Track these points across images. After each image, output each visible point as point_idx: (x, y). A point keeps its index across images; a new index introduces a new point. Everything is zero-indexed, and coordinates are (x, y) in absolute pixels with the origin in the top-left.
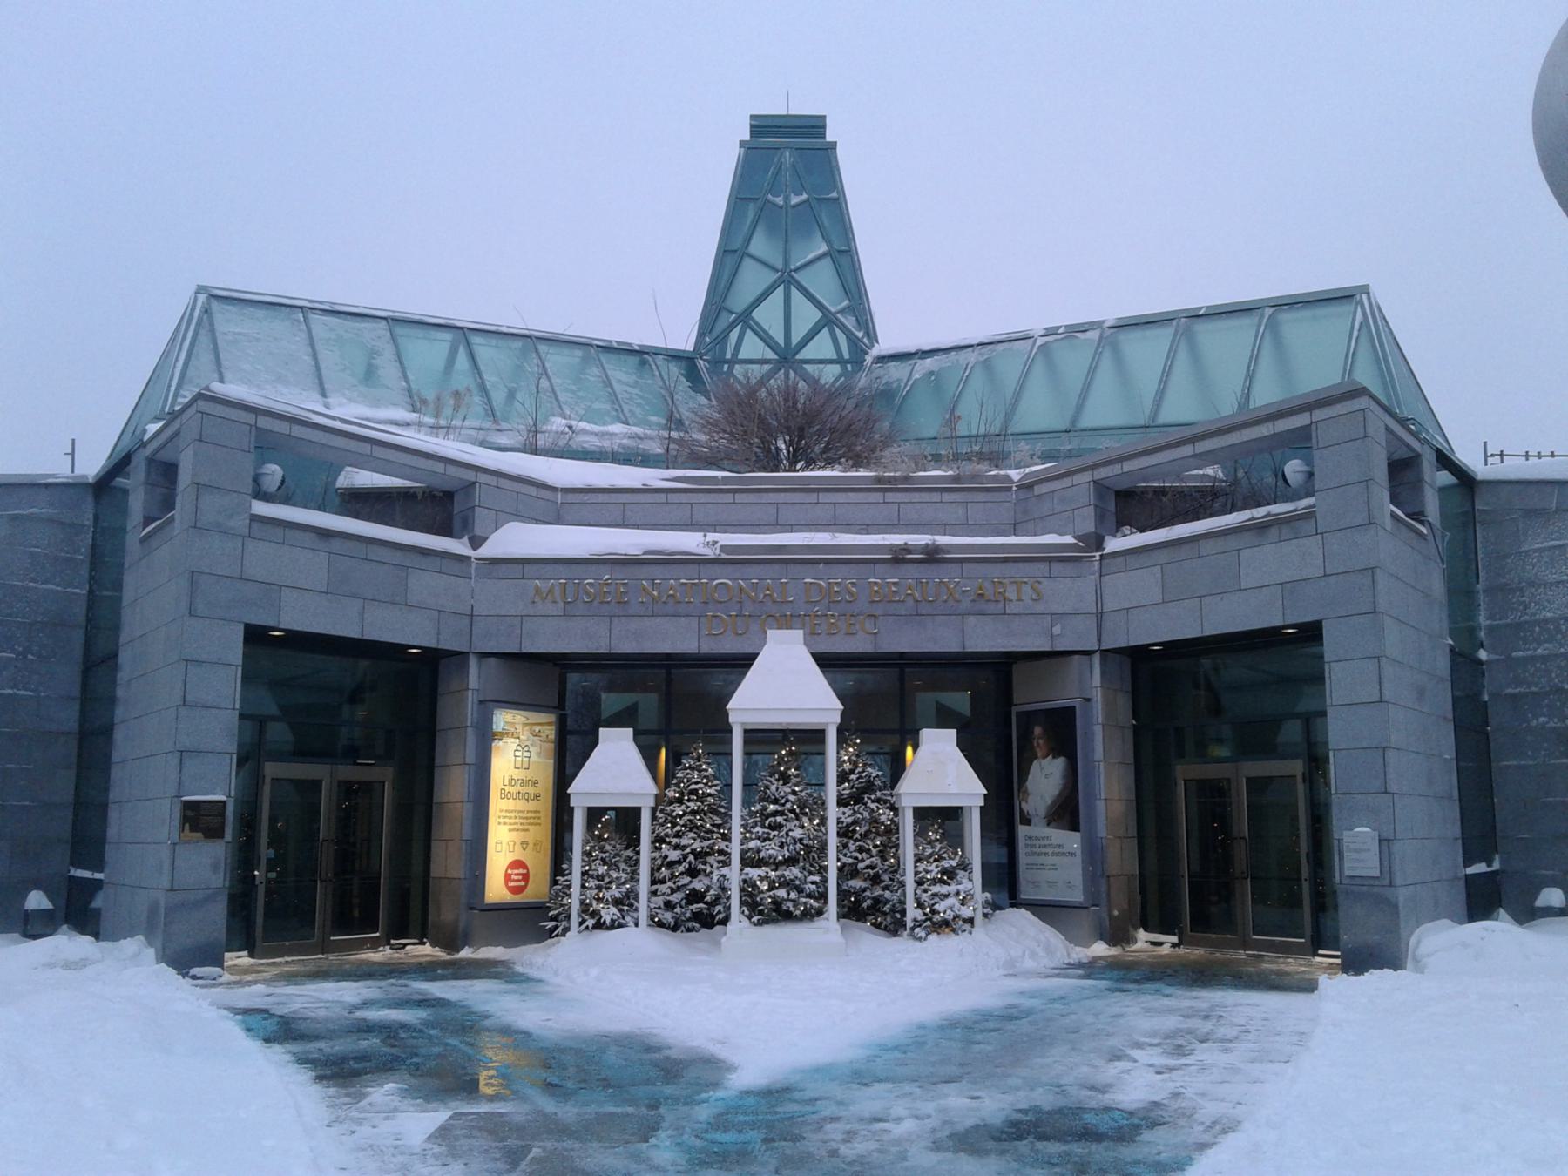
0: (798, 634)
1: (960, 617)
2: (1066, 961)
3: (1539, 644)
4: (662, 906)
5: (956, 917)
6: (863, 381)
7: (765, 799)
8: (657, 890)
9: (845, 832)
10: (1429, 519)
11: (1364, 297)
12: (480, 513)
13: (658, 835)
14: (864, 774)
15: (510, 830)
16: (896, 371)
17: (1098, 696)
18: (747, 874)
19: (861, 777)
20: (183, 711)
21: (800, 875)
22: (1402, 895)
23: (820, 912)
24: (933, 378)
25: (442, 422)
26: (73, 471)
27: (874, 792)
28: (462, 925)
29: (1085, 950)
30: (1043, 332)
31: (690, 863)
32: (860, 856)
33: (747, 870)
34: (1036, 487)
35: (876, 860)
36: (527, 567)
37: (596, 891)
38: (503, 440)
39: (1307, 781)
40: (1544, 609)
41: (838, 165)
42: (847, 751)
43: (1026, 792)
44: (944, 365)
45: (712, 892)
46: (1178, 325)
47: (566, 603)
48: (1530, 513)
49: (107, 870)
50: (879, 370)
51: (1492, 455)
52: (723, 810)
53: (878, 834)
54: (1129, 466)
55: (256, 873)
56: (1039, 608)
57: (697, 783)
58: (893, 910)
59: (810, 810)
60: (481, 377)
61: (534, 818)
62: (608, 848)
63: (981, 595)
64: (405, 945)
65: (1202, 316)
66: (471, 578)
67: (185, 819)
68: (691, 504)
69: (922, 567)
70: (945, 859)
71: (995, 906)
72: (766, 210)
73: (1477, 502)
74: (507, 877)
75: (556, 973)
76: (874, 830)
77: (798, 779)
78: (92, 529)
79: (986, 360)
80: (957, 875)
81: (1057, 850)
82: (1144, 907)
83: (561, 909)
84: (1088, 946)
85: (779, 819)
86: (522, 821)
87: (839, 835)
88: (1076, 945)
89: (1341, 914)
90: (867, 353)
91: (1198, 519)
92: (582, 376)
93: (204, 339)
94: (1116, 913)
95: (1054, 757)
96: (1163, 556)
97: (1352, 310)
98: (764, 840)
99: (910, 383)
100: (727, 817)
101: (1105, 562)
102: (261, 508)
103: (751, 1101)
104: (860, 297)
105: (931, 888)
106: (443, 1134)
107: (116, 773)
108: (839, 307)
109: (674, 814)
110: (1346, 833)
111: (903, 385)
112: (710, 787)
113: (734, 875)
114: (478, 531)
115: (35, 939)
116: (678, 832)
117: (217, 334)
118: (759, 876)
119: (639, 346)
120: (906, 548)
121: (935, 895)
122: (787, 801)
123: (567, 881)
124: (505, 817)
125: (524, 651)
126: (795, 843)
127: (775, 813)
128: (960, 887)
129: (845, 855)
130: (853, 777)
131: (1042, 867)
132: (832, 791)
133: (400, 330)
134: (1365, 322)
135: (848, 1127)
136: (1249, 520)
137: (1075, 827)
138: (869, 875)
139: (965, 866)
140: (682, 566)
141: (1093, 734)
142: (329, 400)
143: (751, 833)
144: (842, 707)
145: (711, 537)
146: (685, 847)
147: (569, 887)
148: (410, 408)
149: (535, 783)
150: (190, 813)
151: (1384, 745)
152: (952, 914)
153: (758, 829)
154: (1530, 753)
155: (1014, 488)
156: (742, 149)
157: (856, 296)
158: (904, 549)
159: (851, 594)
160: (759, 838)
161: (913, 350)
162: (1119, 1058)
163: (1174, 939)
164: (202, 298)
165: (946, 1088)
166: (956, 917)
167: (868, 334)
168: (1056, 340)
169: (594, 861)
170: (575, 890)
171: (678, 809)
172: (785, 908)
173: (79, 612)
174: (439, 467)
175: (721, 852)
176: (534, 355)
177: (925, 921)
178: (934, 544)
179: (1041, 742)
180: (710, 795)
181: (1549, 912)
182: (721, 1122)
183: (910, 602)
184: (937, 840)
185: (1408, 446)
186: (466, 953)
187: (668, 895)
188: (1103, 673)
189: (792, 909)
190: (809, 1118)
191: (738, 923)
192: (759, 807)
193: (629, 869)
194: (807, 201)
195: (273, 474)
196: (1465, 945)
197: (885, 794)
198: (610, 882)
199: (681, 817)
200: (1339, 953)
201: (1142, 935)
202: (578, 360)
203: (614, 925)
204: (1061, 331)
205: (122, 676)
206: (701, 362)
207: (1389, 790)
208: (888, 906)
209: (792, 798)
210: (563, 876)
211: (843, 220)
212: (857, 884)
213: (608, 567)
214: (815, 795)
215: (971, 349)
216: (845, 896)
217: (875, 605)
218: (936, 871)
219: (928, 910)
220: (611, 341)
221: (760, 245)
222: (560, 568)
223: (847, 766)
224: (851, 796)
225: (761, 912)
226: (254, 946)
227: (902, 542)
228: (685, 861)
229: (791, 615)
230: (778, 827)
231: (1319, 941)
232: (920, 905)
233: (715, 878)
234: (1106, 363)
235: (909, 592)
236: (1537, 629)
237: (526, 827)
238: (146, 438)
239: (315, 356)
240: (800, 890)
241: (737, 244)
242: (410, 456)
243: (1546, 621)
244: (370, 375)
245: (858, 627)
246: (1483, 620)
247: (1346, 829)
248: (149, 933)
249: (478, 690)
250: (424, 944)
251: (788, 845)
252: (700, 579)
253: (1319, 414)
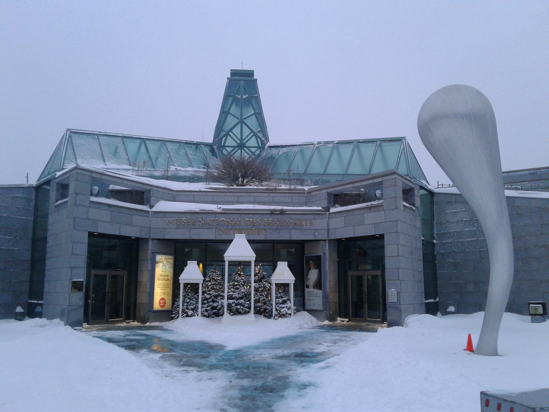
1: (289, 230)
2: (316, 325)
6: (264, 154)
7: (234, 281)
9: (256, 290)
10: (416, 205)
11: (404, 140)
12: (152, 198)
13: (203, 291)
14: (262, 274)
15: (161, 289)
16: (274, 151)
17: (327, 252)
18: (229, 302)
21: (243, 302)
22: (403, 307)
23: (249, 312)
25: (140, 169)
26: (27, 183)
27: (265, 279)
29: (323, 323)
31: (213, 299)
32: (260, 297)
33: (229, 300)
34: (312, 193)
35: (265, 298)
36: (166, 214)
38: (157, 174)
42: (257, 267)
45: (219, 307)
48: (448, 202)
51: (440, 185)
52: (222, 284)
53: (266, 290)
54: (337, 189)
55: (89, 301)
56: (312, 228)
57: (215, 276)
58: (269, 312)
59: (247, 284)
60: (149, 154)
61: (167, 286)
62: (190, 294)
63: (296, 224)
64: (130, 322)
67: (73, 286)
69: (280, 215)
70: (283, 297)
71: (298, 311)
73: (434, 199)
74: (160, 303)
76: (264, 290)
79: (301, 150)
80: (287, 302)
81: (316, 295)
83: (176, 311)
84: (323, 321)
85: (238, 286)
86: (164, 287)
87: (254, 291)
88: (320, 321)
89: (387, 312)
93: (70, 146)
96: (345, 214)
98: (234, 292)
99: (278, 155)
100: (223, 286)
102: (93, 199)
103: (231, 352)
104: (264, 127)
106: (161, 357)
107: (47, 273)
108: (257, 131)
109: (208, 285)
111: (276, 156)
112: (218, 277)
113: (225, 302)
114: (152, 204)
116: (209, 290)
117: (73, 144)
118: (232, 302)
119: (196, 142)
120: (275, 210)
121: (281, 307)
122: (240, 281)
125: (165, 238)
126: (242, 293)
127: (237, 285)
129: (256, 296)
130: (259, 275)
131: (311, 300)
132: (253, 279)
133: (125, 140)
134: (403, 148)
135: (254, 356)
137: (320, 289)
138: (263, 302)
143: (230, 290)
144: (256, 256)
145: (220, 206)
146: (211, 294)
148: (129, 164)
149: (168, 276)
151: (399, 267)
152: (285, 312)
153: (232, 289)
155: (306, 193)
157: (262, 127)
159: (259, 223)
160: (232, 292)
162: (320, 344)
163: (347, 320)
164: (68, 132)
166: (286, 313)
167: (266, 139)
168: (321, 146)
172: (239, 311)
173: (31, 224)
174: (141, 186)
175: (222, 296)
180: (218, 279)
182: (225, 355)
183: (276, 225)
184: (281, 292)
187: (206, 308)
188: (329, 246)
189: (241, 311)
190: (245, 354)
191: (226, 315)
192: (232, 283)
193: (196, 300)
195: (96, 189)
196: (419, 320)
197: (268, 280)
199: (210, 286)
200: (387, 323)
203: (191, 316)
206: (215, 146)
208: (268, 310)
209: (242, 281)
212: (259, 304)
215: (296, 146)
218: (281, 301)
219: (279, 311)
220: (187, 141)
221: (234, 110)
222: (175, 214)
224: (258, 280)
225: (233, 312)
226: (89, 322)
227: (273, 208)
228: (211, 298)
230: (238, 289)
231: (384, 320)
232: (276, 310)
233: (220, 303)
234: (335, 152)
237: (165, 288)
238: (56, 177)
239: (101, 149)
240: (243, 306)
241: (226, 110)
242: (134, 183)
243: (451, 232)
244: (115, 153)
246: (435, 232)
247: (389, 290)
248: (61, 319)
250: (135, 322)
251: (240, 294)
252: (216, 218)
253: (384, 178)
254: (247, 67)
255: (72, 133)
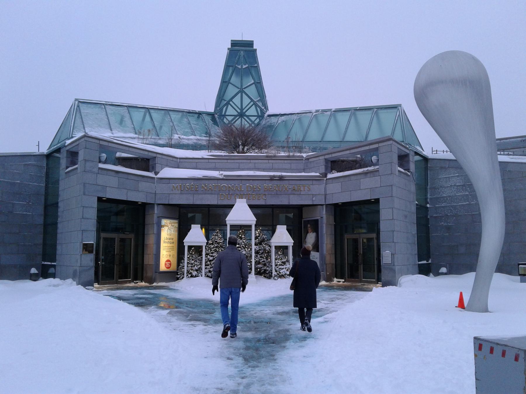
0: (245, 200)
3: (443, 203)
4: (208, 271)
5: (285, 274)
6: (263, 122)
8: (206, 268)
9: (257, 252)
10: (411, 171)
11: (400, 107)
13: (207, 253)
14: (262, 237)
15: (166, 252)
16: (274, 120)
19: (261, 238)
20: (83, 220)
22: (397, 268)
24: (284, 123)
25: (145, 137)
26: (39, 151)
27: (265, 242)
28: (153, 278)
30: (315, 111)
32: (261, 259)
35: (265, 260)
37: (191, 267)
39: (100, 237)
40: (444, 194)
41: (257, 57)
43: (306, 242)
44: (287, 119)
46: (352, 111)
47: (181, 190)
48: (442, 168)
49: (57, 262)
50: (269, 119)
51: (434, 151)
52: (224, 246)
53: (266, 253)
54: (334, 155)
55: (99, 262)
56: (310, 193)
57: (217, 239)
58: (269, 272)
59: (248, 247)
60: (154, 123)
61: (172, 248)
62: (194, 256)
64: (137, 282)
65: (358, 110)
66: (155, 183)
67: (84, 248)
68: (215, 163)
72: (235, 70)
74: (166, 264)
75: (182, 288)
77: (244, 238)
78: (46, 167)
79: (299, 118)
82: (336, 271)
86: (169, 249)
87: (255, 253)
90: (265, 114)
91: (352, 170)
92: (182, 121)
93: (78, 115)
94: (328, 274)
95: (313, 233)
96: (341, 180)
97: (396, 111)
99: (277, 124)
101: (327, 181)
102: (101, 166)
105: (279, 267)
106: (169, 313)
107: (59, 236)
110: (384, 252)
111: (275, 124)
112: (221, 240)
114: (157, 170)
115: (36, 281)
116: (212, 252)
117: (82, 113)
119: (198, 111)
120: (274, 176)
121: (280, 268)
122: (242, 244)
123: (183, 265)
124: (165, 248)
125: (170, 203)
128: (287, 266)
129: (257, 258)
130: (259, 238)
132: (253, 241)
133: (130, 109)
134: (399, 115)
135: (255, 312)
136: (363, 171)
137: (318, 251)
139: (288, 261)
140: (213, 180)
141: (323, 227)
142: (113, 132)
144: (256, 220)
145: (221, 172)
146: (214, 256)
147: (184, 266)
148: (135, 133)
149: (173, 239)
150: (85, 247)
154: (439, 232)
155: (304, 159)
156: (229, 51)
158: (273, 177)
159: (259, 188)
161: (278, 114)
163: (343, 280)
164: (77, 102)
165: (277, 306)
166: (285, 274)
167: (265, 108)
169: (190, 260)
170: (186, 267)
171: (212, 246)
173: (43, 191)
176: (168, 116)
177: (277, 275)
178: (281, 175)
179: (310, 229)
180: (221, 242)
181: (443, 274)
183: (275, 191)
184: (281, 254)
185: (405, 152)
186: (155, 284)
187: (210, 269)
193: (199, 262)
194: (248, 67)
198: (195, 265)
199: (213, 248)
200: (381, 283)
201: (335, 279)
202: (180, 116)
203: (196, 276)
204: (320, 111)
205: (60, 210)
206: (216, 115)
207: (394, 241)
208: (268, 271)
209: (243, 243)
210: (182, 264)
211: (258, 73)
212: (260, 266)
213: (193, 181)
214: (249, 243)
215: (295, 115)
216: (257, 269)
217: (265, 192)
218: (280, 262)
219: (278, 272)
220: (190, 110)
221: (234, 80)
222: (180, 181)
223: (258, 235)
224: (258, 243)
226: (99, 282)
227: (273, 175)
228: (214, 260)
229: (243, 194)
231: (379, 280)
232: (276, 271)
234: (332, 120)
235: (275, 188)
236: (442, 199)
238: (66, 145)
239: (108, 118)
241: (227, 80)
243: (444, 197)
245: (261, 197)
246: (429, 196)
249: (157, 214)
250: (142, 282)
252: (218, 184)
253: (381, 145)
254: (246, 38)
255: (81, 103)
